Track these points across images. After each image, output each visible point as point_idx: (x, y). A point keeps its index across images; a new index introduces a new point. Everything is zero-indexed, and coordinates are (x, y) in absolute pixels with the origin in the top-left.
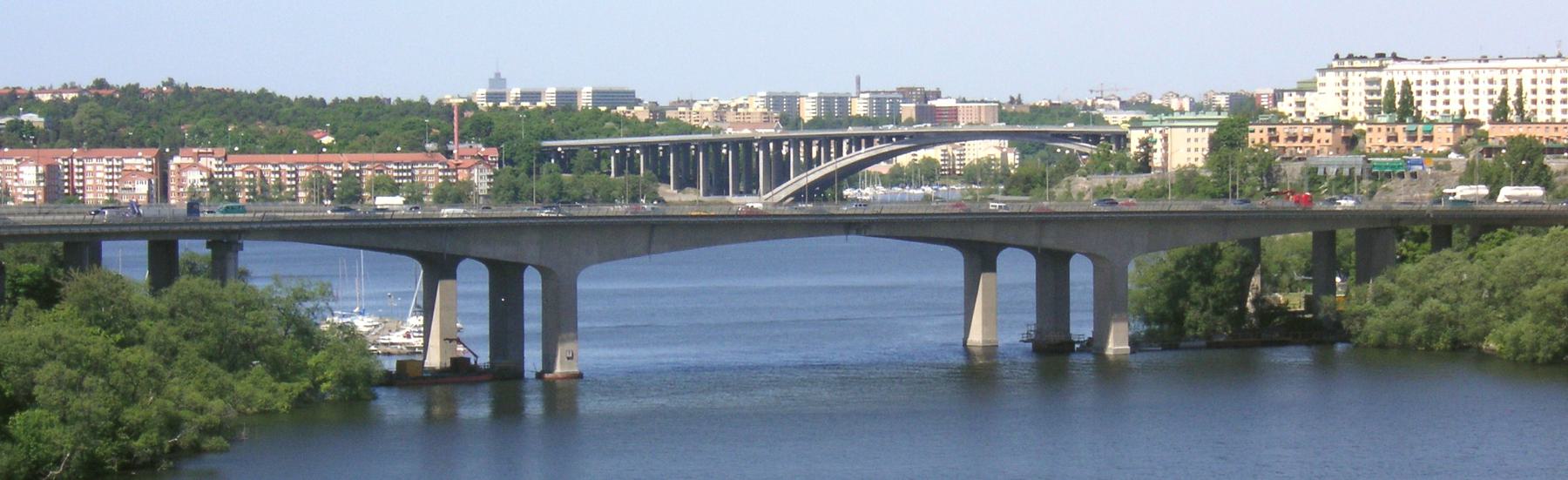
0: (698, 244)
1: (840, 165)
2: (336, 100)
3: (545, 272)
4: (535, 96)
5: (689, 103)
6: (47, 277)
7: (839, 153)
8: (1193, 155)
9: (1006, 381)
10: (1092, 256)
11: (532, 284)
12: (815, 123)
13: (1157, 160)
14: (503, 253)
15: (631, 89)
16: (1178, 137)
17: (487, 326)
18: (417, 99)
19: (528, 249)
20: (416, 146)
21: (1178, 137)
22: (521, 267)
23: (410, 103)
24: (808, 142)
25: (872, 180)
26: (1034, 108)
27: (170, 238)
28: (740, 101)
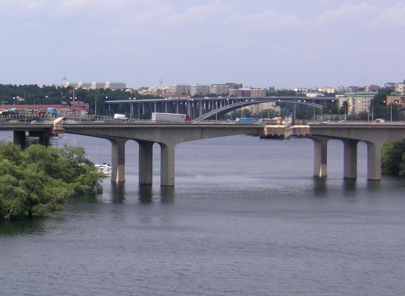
0: (221, 135)
1: (219, 111)
2: (20, 86)
3: (163, 146)
4: (90, 85)
5: (147, 89)
6: (347, 101)
7: (219, 107)
8: (364, 108)
9: (358, 190)
10: (368, 143)
11: (156, 150)
12: (196, 96)
13: (350, 109)
14: (146, 137)
15: (124, 83)
16: (359, 101)
17: (138, 168)
18: (51, 85)
19: (157, 137)
20: (58, 103)
21: (359, 101)
22: (152, 143)
23: (48, 87)
24: (207, 101)
25: (229, 117)
26: (279, 91)
27: (22, 130)
28: (166, 88)
